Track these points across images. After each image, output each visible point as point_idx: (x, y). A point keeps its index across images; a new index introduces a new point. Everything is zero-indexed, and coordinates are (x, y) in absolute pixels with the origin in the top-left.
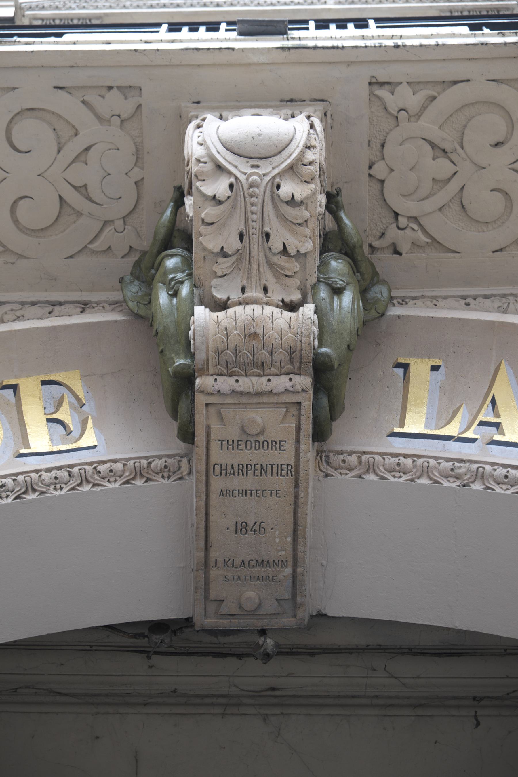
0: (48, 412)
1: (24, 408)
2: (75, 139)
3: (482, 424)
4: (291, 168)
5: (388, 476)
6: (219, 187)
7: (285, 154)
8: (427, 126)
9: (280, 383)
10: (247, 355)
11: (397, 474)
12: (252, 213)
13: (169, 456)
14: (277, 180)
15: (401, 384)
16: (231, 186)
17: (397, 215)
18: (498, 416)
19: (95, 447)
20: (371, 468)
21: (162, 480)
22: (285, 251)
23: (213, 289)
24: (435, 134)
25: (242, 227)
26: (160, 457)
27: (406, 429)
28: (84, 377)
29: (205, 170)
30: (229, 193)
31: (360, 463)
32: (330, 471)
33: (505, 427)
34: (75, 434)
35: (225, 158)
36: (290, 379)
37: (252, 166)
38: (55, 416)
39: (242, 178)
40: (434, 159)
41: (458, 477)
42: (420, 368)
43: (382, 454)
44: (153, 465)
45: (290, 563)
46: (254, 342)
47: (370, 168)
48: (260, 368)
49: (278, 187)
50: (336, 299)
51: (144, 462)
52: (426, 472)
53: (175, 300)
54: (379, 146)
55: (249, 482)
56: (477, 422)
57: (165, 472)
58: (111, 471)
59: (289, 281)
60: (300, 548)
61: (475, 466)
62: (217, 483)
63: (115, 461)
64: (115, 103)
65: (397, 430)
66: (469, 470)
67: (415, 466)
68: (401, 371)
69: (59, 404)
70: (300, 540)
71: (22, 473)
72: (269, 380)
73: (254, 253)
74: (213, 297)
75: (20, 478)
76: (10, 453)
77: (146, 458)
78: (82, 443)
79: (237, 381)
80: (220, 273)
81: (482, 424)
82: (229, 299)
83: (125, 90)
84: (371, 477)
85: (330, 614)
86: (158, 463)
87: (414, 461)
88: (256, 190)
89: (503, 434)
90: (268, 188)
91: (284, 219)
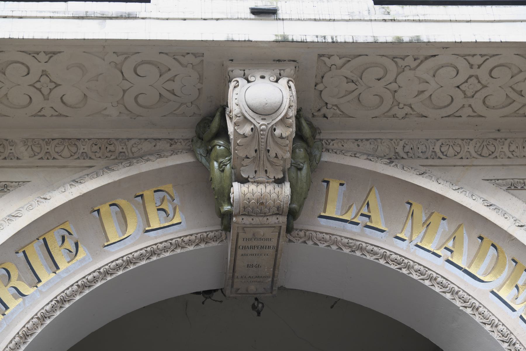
0: (157, 205)
1: (146, 205)
2: (169, 72)
3: (362, 215)
4: (282, 120)
5: (318, 242)
6: (247, 129)
7: (278, 113)
8: (346, 71)
9: (273, 220)
10: (258, 208)
11: (322, 242)
12: (262, 139)
13: (217, 231)
14: (274, 127)
15: (325, 190)
16: (252, 129)
17: (327, 104)
18: (370, 212)
19: (180, 223)
20: (310, 238)
21: (213, 243)
22: (276, 157)
23: (241, 172)
24: (349, 74)
25: (257, 148)
26: (212, 231)
27: (326, 214)
28: (174, 186)
29: (240, 121)
30: (251, 133)
31: (305, 235)
32: (292, 238)
33: (373, 218)
34: (171, 216)
35: (249, 115)
36: (277, 218)
37: (262, 119)
38: (161, 207)
39: (258, 126)
40: (347, 83)
41: (350, 247)
42: (334, 185)
43: (316, 232)
44: (209, 236)
45: (271, 277)
46: (262, 206)
47: (316, 86)
48: (265, 215)
49: (275, 130)
50: (299, 172)
51: (205, 234)
52: (335, 243)
53: (222, 174)
54: (320, 77)
55: (255, 251)
56: (360, 214)
57: (215, 239)
58: (190, 240)
59: (277, 167)
60: (276, 272)
61: (358, 243)
62: (240, 252)
63: (191, 235)
64: (190, 59)
65: (323, 214)
66: (355, 245)
67: (330, 239)
68: (325, 184)
69: (163, 200)
70: (276, 270)
71: (149, 246)
72: (267, 219)
73: (262, 158)
74: (242, 176)
75: (149, 249)
76: (141, 231)
77: (206, 232)
78: (175, 221)
79: (253, 219)
80: (245, 165)
81: (362, 215)
82: (249, 177)
83: (195, 55)
84: (310, 243)
85: (288, 286)
86: (211, 235)
87: (330, 237)
88: (264, 133)
89: (371, 222)
90: (270, 132)
91: (276, 143)
